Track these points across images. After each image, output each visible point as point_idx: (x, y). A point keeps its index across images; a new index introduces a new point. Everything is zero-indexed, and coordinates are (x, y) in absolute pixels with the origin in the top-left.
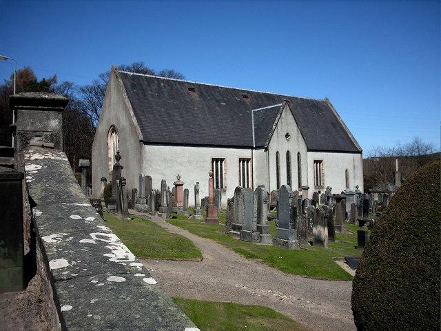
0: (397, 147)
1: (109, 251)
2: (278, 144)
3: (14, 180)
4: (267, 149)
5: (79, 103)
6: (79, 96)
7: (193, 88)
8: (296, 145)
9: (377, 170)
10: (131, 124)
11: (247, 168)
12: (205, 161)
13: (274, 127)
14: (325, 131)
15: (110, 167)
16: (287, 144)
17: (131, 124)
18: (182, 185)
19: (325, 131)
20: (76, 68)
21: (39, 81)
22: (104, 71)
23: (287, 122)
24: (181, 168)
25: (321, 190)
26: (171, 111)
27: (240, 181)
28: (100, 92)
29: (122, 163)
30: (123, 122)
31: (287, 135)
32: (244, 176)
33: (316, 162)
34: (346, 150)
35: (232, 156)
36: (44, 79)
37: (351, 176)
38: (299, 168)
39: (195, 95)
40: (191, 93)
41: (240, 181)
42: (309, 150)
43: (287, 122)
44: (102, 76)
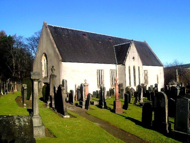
0: (167, 65)
5: (25, 45)
6: (26, 43)
8: (138, 63)
9: (170, 74)
10: (55, 52)
11: (114, 75)
14: (148, 57)
15: (43, 76)
17: (55, 52)
19: (148, 57)
20: (23, 29)
22: (37, 31)
23: (133, 52)
24: (79, 75)
26: (74, 46)
27: (97, 73)
28: (36, 41)
29: (55, 73)
30: (50, 52)
31: (133, 58)
36: (10, 35)
38: (139, 72)
41: (97, 73)
44: (36, 33)
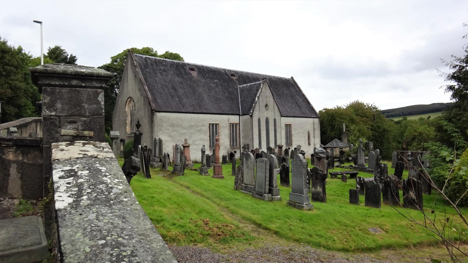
1: (65, 53)
2: (259, 113)
3: (14, 248)
4: (251, 116)
7: (193, 68)
8: (272, 113)
12: (203, 125)
13: (256, 99)
16: (266, 112)
18: (189, 146)
21: (447, 98)
25: (290, 147)
31: (266, 106)
32: (233, 139)
33: (287, 125)
34: (296, 116)
35: (224, 121)
37: (312, 136)
39: (194, 74)
40: (192, 72)
42: (282, 116)
43: (265, 95)
